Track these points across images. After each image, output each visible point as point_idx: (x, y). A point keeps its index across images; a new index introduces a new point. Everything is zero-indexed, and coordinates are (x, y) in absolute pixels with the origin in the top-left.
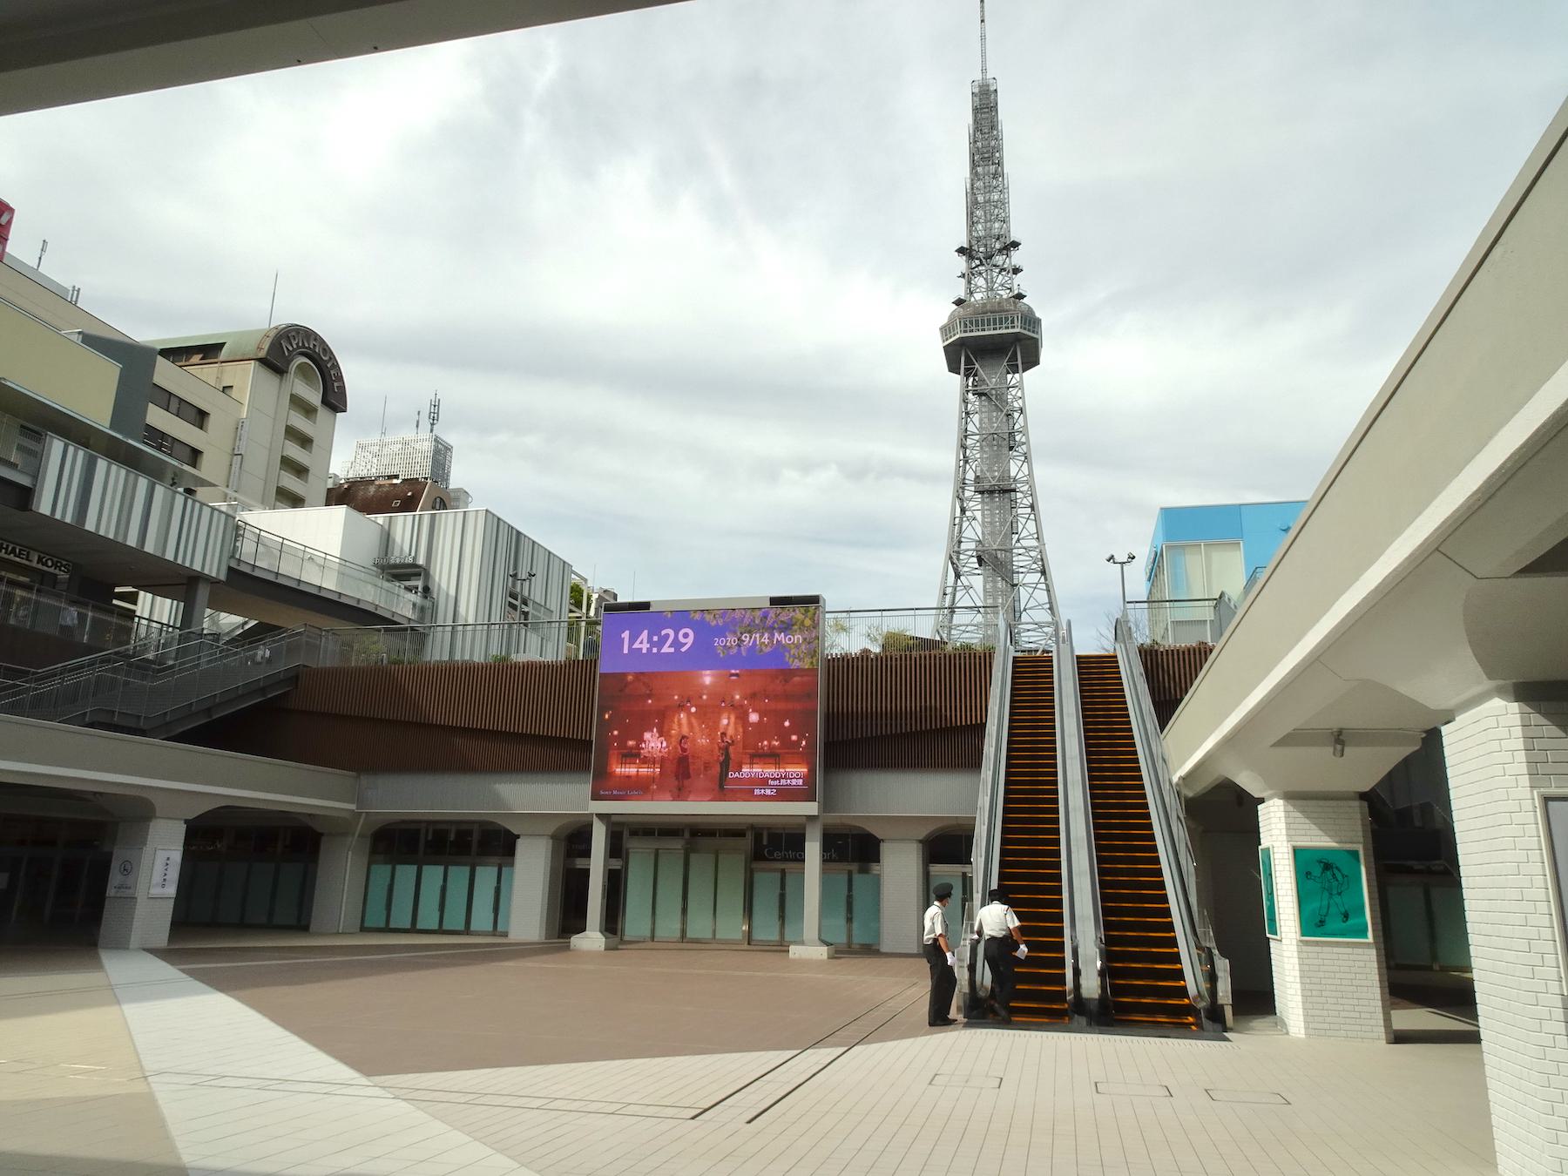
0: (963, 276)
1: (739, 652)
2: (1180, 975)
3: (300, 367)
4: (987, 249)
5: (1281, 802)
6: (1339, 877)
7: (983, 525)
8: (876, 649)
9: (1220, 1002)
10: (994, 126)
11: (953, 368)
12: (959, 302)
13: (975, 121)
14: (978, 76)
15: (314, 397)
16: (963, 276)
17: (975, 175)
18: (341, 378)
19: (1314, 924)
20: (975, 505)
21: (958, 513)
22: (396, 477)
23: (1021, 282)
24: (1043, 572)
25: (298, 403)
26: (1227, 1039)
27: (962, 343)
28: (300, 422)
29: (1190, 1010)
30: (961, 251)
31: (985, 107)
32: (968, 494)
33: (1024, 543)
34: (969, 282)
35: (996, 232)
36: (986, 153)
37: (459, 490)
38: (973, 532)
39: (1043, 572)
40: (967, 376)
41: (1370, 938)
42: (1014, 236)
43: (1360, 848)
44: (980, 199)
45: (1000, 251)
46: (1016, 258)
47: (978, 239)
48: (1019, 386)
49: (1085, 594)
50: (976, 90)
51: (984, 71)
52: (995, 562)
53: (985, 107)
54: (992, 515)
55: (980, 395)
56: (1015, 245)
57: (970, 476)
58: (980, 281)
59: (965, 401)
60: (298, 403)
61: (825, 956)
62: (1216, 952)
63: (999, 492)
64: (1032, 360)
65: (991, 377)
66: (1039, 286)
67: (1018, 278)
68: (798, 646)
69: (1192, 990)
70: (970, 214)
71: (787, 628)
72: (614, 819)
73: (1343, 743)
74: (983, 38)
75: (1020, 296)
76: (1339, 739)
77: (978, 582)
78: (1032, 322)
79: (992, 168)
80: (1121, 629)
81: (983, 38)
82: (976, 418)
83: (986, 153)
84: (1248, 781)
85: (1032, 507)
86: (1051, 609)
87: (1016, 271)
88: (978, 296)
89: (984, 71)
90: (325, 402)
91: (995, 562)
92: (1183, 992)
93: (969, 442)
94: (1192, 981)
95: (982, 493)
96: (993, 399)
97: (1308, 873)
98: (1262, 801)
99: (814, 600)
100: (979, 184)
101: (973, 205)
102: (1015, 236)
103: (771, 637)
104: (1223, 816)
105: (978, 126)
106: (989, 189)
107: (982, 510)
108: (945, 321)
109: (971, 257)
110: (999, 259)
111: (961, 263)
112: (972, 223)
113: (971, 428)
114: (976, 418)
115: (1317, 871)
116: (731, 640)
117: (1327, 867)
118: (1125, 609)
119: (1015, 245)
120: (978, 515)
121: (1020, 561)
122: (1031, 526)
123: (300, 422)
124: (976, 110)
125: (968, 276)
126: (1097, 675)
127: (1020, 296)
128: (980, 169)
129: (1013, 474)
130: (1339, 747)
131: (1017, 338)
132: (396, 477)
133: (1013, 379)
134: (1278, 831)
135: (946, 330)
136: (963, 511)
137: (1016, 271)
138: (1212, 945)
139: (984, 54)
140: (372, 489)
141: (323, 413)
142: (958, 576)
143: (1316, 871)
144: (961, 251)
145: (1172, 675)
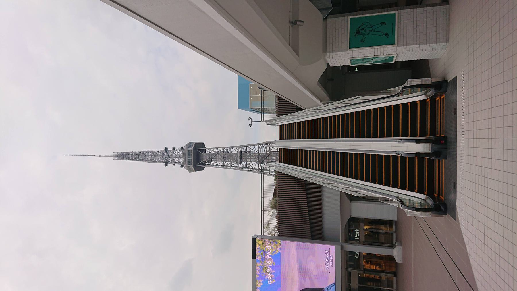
2: (414, 104)
4: (166, 157)
5: (328, 54)
6: (363, 27)
7: (251, 162)
8: (276, 213)
9: (430, 83)
10: (128, 154)
12: (182, 166)
13: (126, 159)
19: (388, 38)
20: (245, 164)
21: (247, 169)
24: (267, 144)
26: (455, 80)
27: (195, 166)
29: (433, 99)
30: (166, 165)
32: (241, 166)
33: (257, 150)
35: (161, 154)
38: (253, 165)
39: (267, 144)
41: (396, 12)
42: (163, 149)
43: (349, 17)
44: (150, 159)
46: (170, 148)
48: (210, 149)
49: (266, 133)
51: (110, 156)
54: (248, 158)
55: (211, 161)
56: (166, 148)
57: (236, 165)
58: (176, 160)
59: (213, 165)
62: (403, 86)
63: (241, 156)
64: (202, 145)
65: (206, 157)
66: (178, 141)
67: (177, 148)
68: (272, 248)
69: (423, 98)
70: (155, 162)
71: (265, 252)
73: (296, 21)
75: (182, 148)
76: (294, 23)
78: (190, 144)
79: (141, 154)
80: (271, 123)
81: (100, 156)
82: (218, 162)
84: (319, 70)
85: (246, 147)
87: (174, 149)
88: (181, 160)
89: (110, 156)
92: (423, 102)
93: (225, 165)
94: (418, 97)
95: (241, 162)
96: (214, 156)
97: (361, 41)
98: (328, 65)
99: (254, 241)
100: (146, 159)
101: (152, 161)
103: (268, 259)
104: (337, 83)
105: (128, 159)
107: (247, 162)
108: (187, 171)
109: (169, 162)
110: (170, 154)
111: (170, 165)
112: (158, 162)
113: (221, 164)
114: (218, 162)
115: (360, 37)
116: (269, 276)
117: (358, 32)
118: (263, 121)
119: (166, 148)
120: (248, 163)
121: (263, 151)
122: (252, 147)
124: (123, 159)
125: (174, 163)
126: (286, 132)
127: (182, 148)
129: (236, 152)
130: (298, 23)
131: (194, 149)
133: (207, 151)
134: (343, 58)
135: (190, 171)
136: (247, 167)
137: (174, 149)
138: (401, 87)
139: (105, 156)
143: (359, 37)
144: (166, 165)
145: (285, 107)
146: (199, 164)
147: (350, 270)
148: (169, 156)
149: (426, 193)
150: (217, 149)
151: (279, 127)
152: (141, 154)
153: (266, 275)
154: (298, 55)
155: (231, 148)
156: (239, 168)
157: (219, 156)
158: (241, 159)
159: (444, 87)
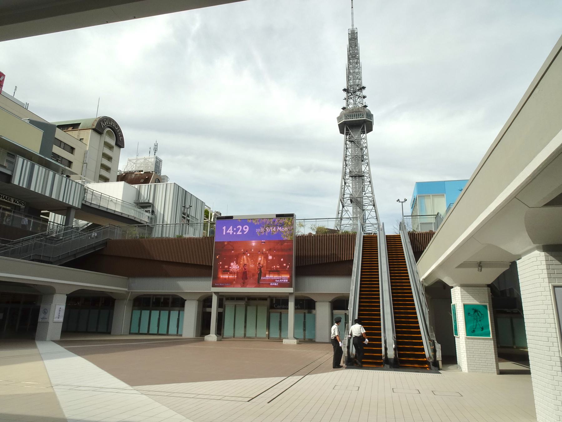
0: (345, 99)
1: (265, 234)
2: (423, 350)
3: (107, 132)
4: (354, 89)
6: (480, 315)
7: (352, 188)
8: (314, 233)
9: (437, 359)
10: (356, 45)
11: (342, 132)
12: (344, 108)
13: (350, 43)
14: (351, 28)
15: (113, 142)
16: (345, 99)
17: (349, 63)
18: (122, 136)
19: (471, 331)
20: (350, 181)
21: (343, 184)
22: (142, 171)
23: (366, 101)
24: (374, 205)
25: (107, 145)
26: (440, 373)
27: (345, 123)
28: (107, 151)
29: (426, 362)
30: (344, 90)
31: (353, 38)
32: (347, 177)
34: (347, 101)
35: (357, 83)
36: (353, 55)
37: (165, 176)
38: (349, 191)
39: (374, 205)
40: (347, 135)
41: (491, 337)
42: (363, 85)
43: (487, 304)
44: (351, 71)
45: (358, 90)
46: (364, 92)
47: (351, 86)
48: (365, 138)
49: (389, 213)
50: (350, 32)
51: (353, 25)
52: (357, 202)
53: (353, 38)
54: (356, 185)
55: (351, 142)
56: (364, 88)
57: (348, 171)
58: (351, 101)
59: (346, 144)
60: (107, 145)
61: (296, 343)
62: (436, 342)
63: (358, 176)
64: (370, 129)
65: (355, 135)
66: (372, 103)
67: (365, 100)
68: (286, 232)
70: (348, 77)
71: (282, 225)
72: (220, 294)
73: (481, 267)
74: (352, 13)
75: (366, 106)
76: (480, 265)
77: (350, 209)
78: (370, 115)
79: (356, 60)
80: (402, 226)
81: (352, 13)
82: (350, 150)
83: (353, 55)
84: (447, 280)
85: (370, 182)
86: (377, 218)
87: (364, 97)
88: (351, 106)
89: (353, 25)
90: (116, 144)
91: (357, 202)
92: (424, 356)
93: (347, 159)
94: (427, 352)
95: (352, 177)
96: (356, 143)
98: (452, 287)
99: (292, 215)
100: (351, 66)
101: (349, 74)
102: (364, 85)
103: (276, 229)
104: (438, 293)
105: (351, 45)
106: (354, 68)
107: (352, 183)
108: (339, 115)
109: (348, 92)
110: (358, 93)
111: (345, 94)
112: (348, 80)
113: (348, 153)
114: (350, 150)
115: (472, 313)
116: (262, 230)
117: (476, 311)
118: (403, 219)
119: (364, 88)
120: (351, 185)
121: (366, 201)
122: (370, 189)
123: (107, 151)
124: (350, 40)
125: (347, 99)
126: (393, 242)
127: (366, 106)
128: (351, 61)
129: (363, 170)
130: (480, 268)
131: (365, 121)
132: (142, 171)
133: (363, 136)
134: (458, 298)
135: (339, 119)
136: (345, 183)
137: (364, 97)
140: (133, 176)
141: (116, 148)
142: (343, 207)
143: (472, 313)
144: (344, 90)
145: (420, 242)
146: (347, 130)
147: (269, 299)
148: (355, 92)
149: (344, 365)
150: (366, 147)
151: (398, 234)
152: (356, 60)
153: (263, 227)
154: (457, 267)
155: (368, 164)
156: (345, 174)
157: (358, 152)
158: (355, 177)
159: (432, 366)
